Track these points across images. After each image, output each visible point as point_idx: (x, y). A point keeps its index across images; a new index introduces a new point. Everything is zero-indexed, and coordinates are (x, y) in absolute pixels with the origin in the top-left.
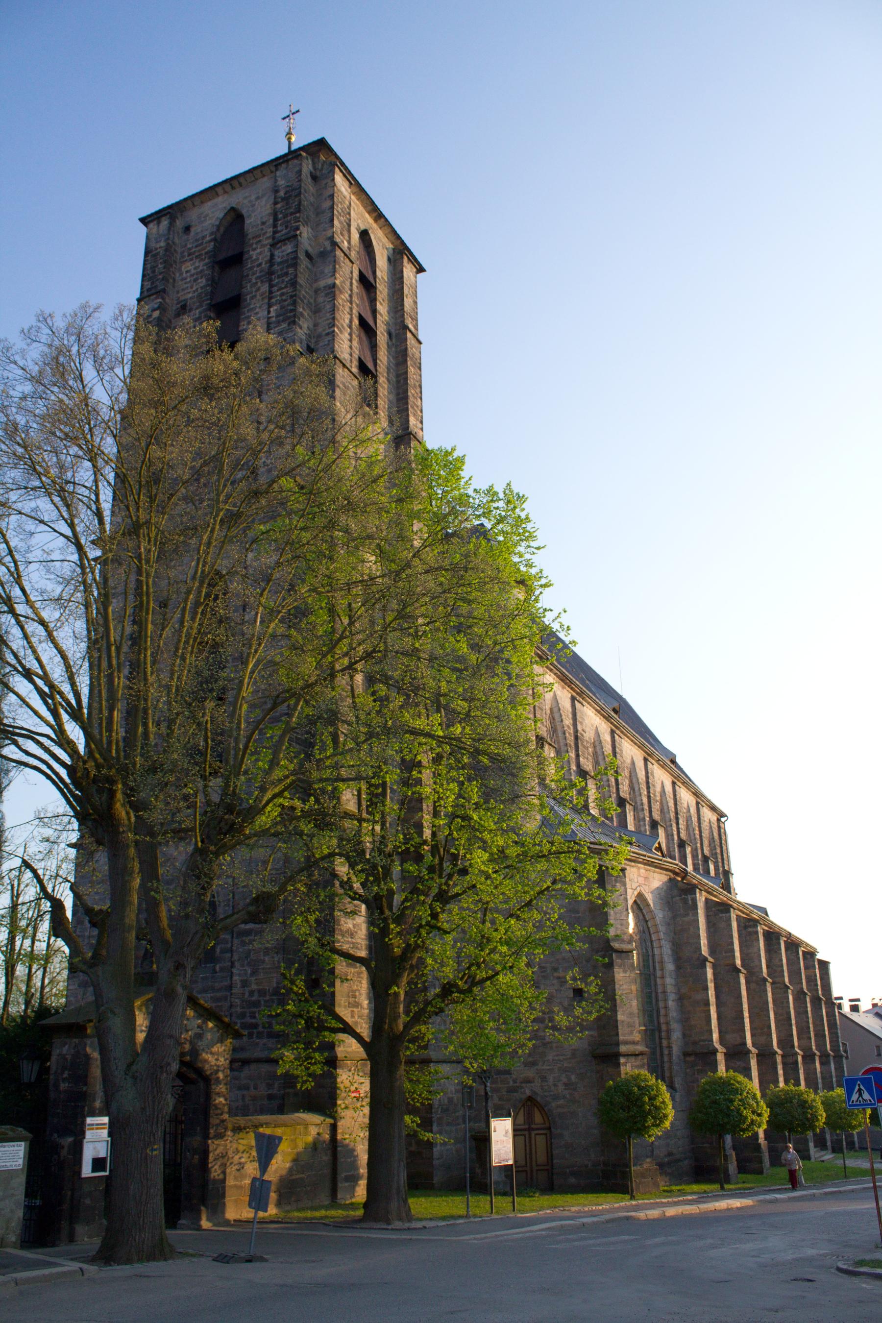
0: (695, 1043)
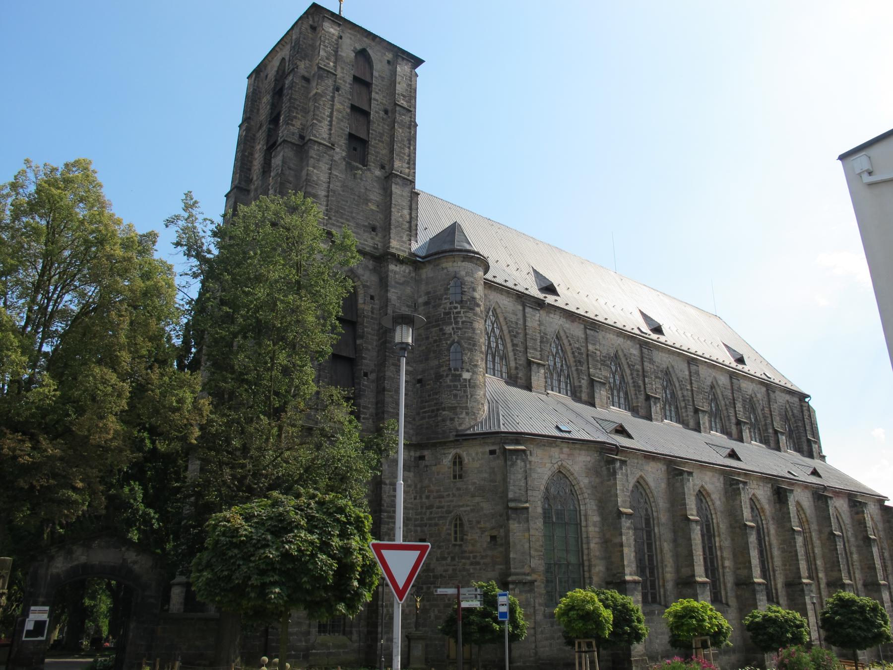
0: (614, 575)
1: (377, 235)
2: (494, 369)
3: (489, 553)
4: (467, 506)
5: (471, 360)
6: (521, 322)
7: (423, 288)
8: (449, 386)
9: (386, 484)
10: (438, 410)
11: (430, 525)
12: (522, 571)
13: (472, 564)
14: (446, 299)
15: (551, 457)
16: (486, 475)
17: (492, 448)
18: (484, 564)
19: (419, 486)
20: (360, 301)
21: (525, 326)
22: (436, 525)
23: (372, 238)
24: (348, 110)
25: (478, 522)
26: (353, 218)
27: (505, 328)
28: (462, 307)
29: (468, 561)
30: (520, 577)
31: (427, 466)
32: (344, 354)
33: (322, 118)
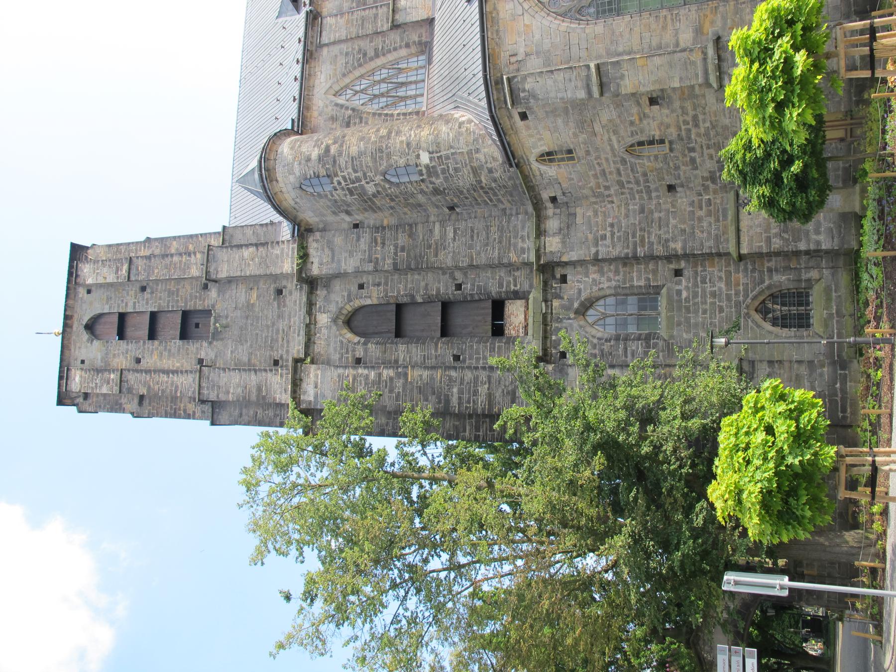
1: (285, 287)
2: (416, 82)
3: (677, 104)
4: (610, 140)
5: (403, 154)
6: (344, 47)
7: (330, 218)
8: (446, 179)
9: (597, 253)
10: (482, 188)
11: (647, 181)
12: (699, 64)
13: (697, 125)
14: (332, 196)
15: (514, 17)
16: (560, 121)
17: (517, 118)
18: (695, 109)
19: (593, 200)
20: (368, 302)
21: (346, 40)
22: (645, 175)
23: (291, 293)
24: (156, 342)
25: (632, 123)
26: (273, 324)
27: (357, 73)
28: (336, 175)
29: (694, 131)
30: (711, 68)
31: (564, 194)
32: (439, 318)
33: (172, 384)
